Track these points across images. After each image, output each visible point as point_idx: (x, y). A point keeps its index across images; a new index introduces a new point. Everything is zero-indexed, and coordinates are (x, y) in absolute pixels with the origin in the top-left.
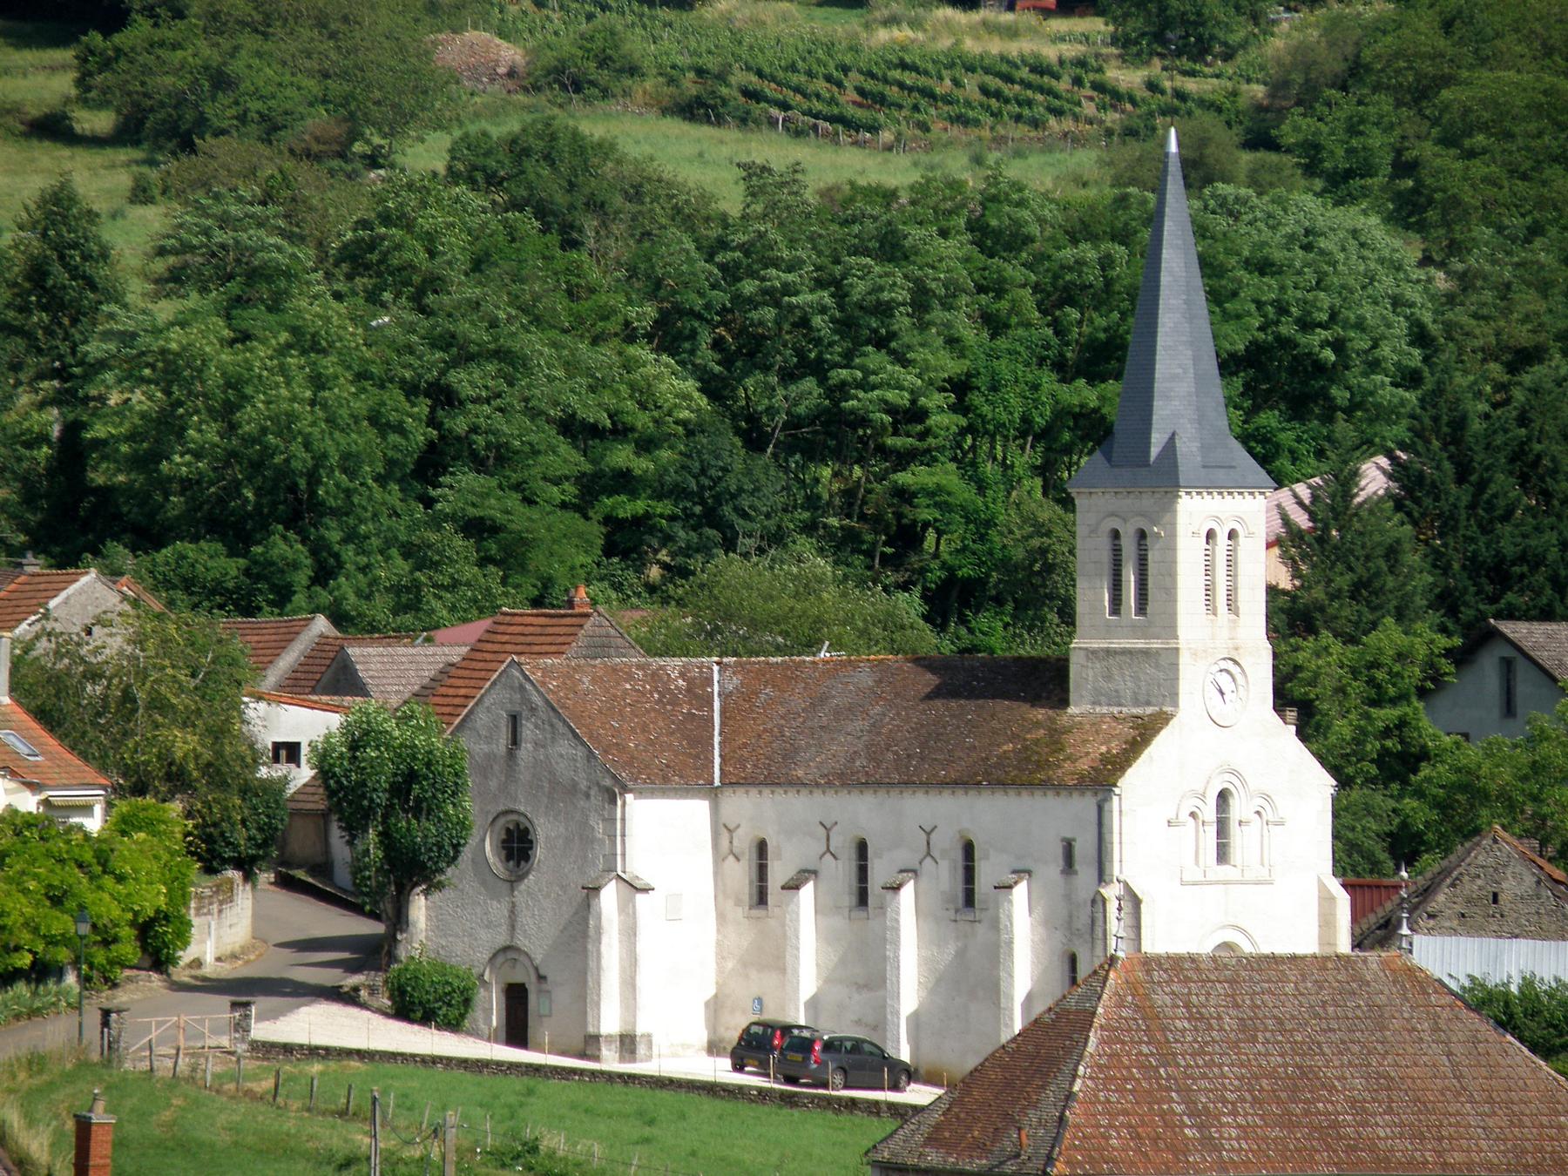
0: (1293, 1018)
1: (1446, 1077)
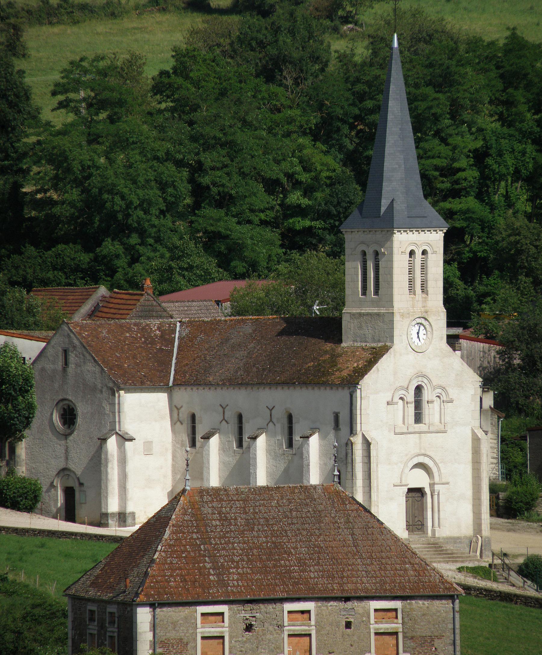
0: (274, 518)
1: (349, 546)
